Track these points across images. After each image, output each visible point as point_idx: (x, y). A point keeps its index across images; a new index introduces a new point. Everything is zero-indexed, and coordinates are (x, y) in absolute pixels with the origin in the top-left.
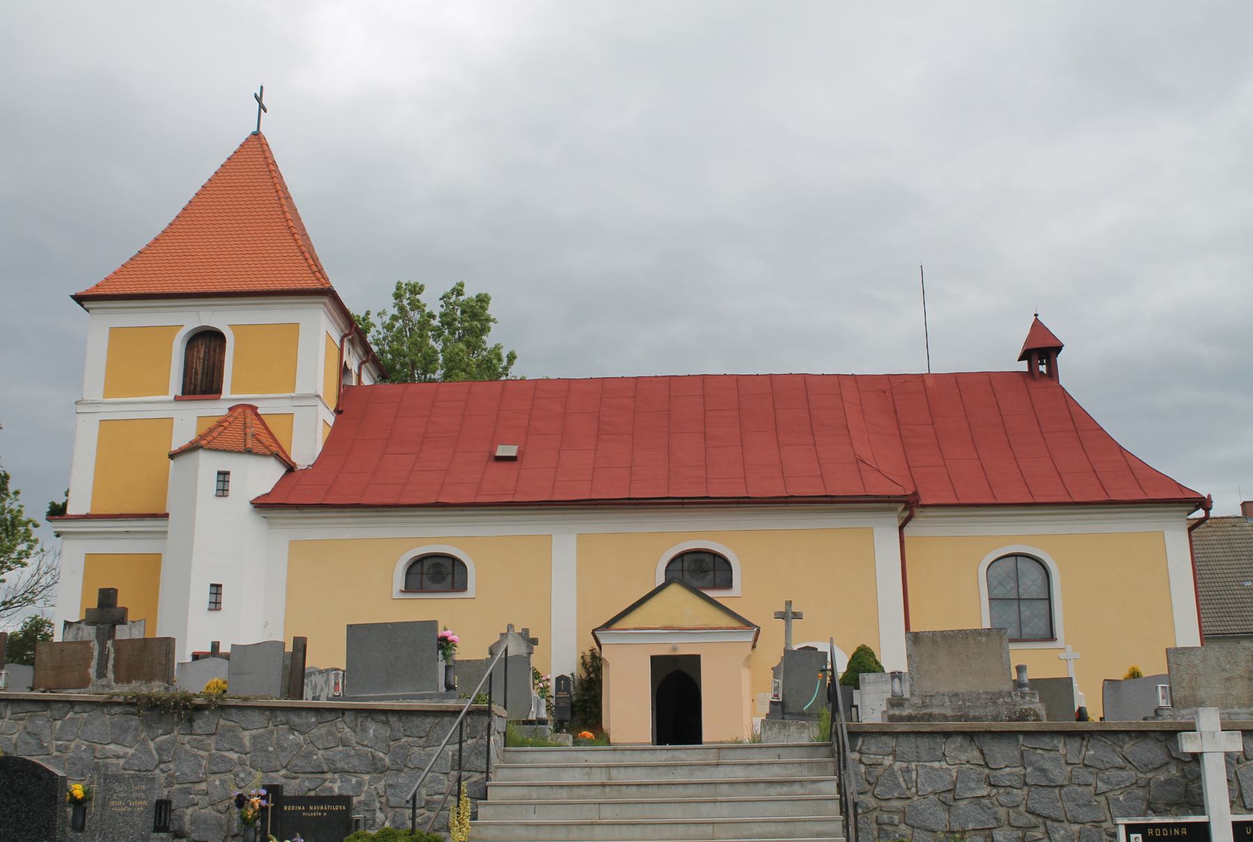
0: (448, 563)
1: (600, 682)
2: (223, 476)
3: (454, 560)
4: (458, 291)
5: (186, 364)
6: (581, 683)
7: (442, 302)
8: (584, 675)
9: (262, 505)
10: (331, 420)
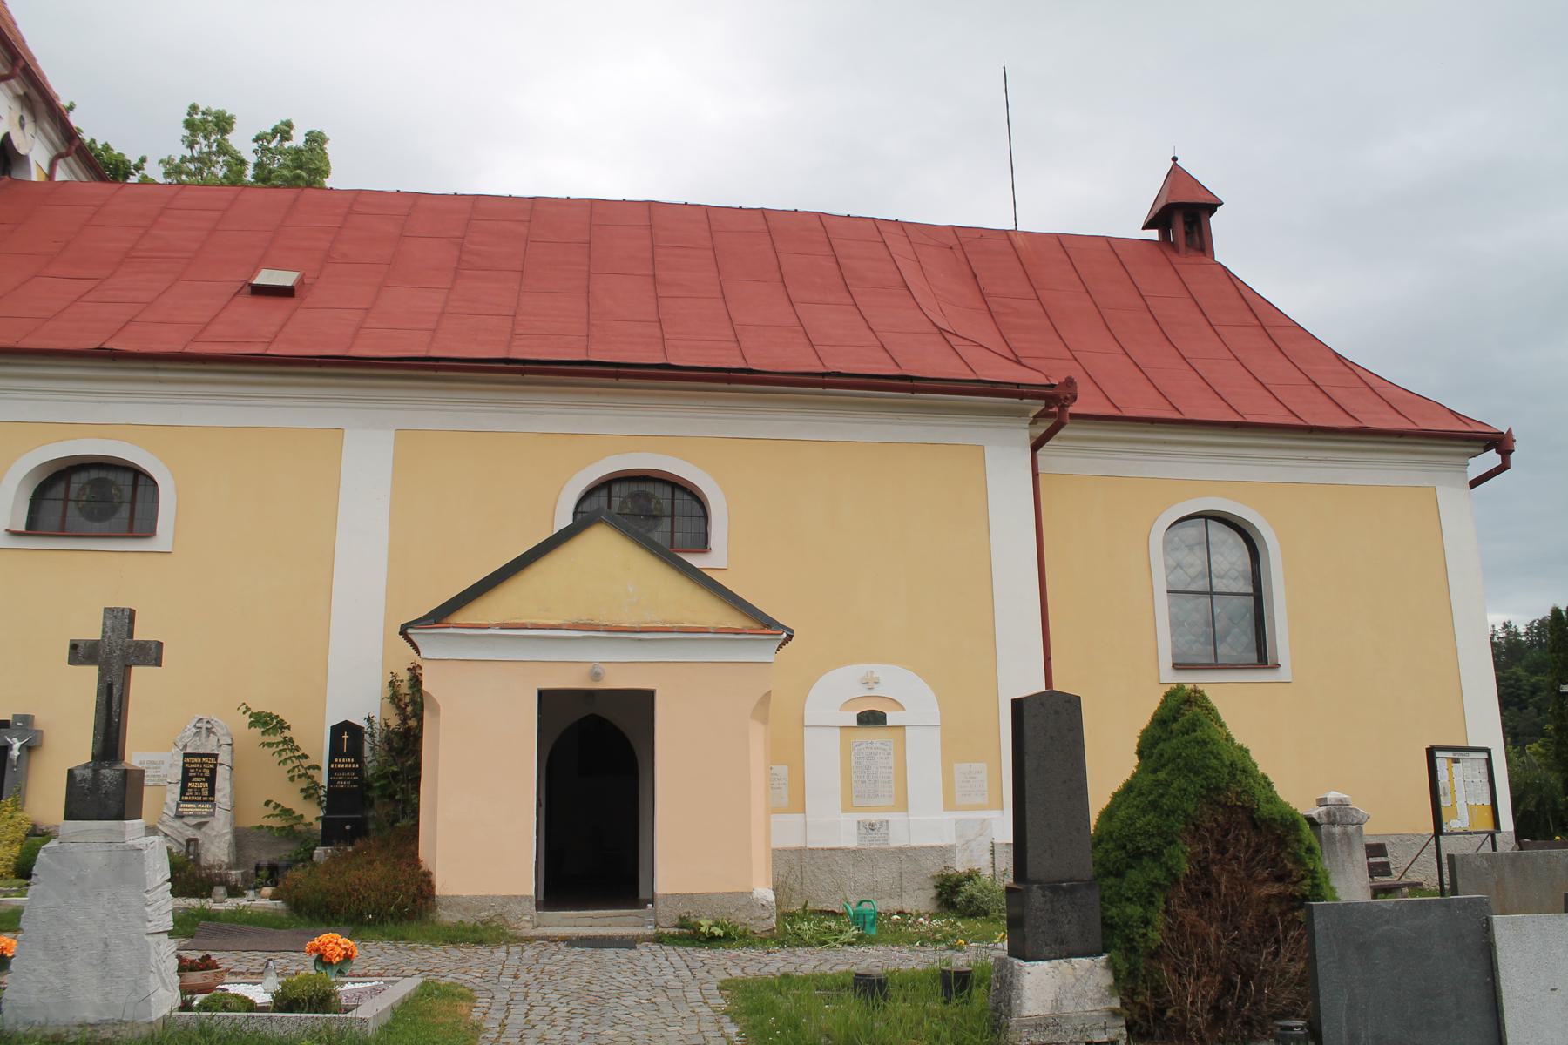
1: (418, 738)
3: (138, 475)
4: (284, 131)
6: (388, 740)
7: (256, 146)
8: (394, 722)
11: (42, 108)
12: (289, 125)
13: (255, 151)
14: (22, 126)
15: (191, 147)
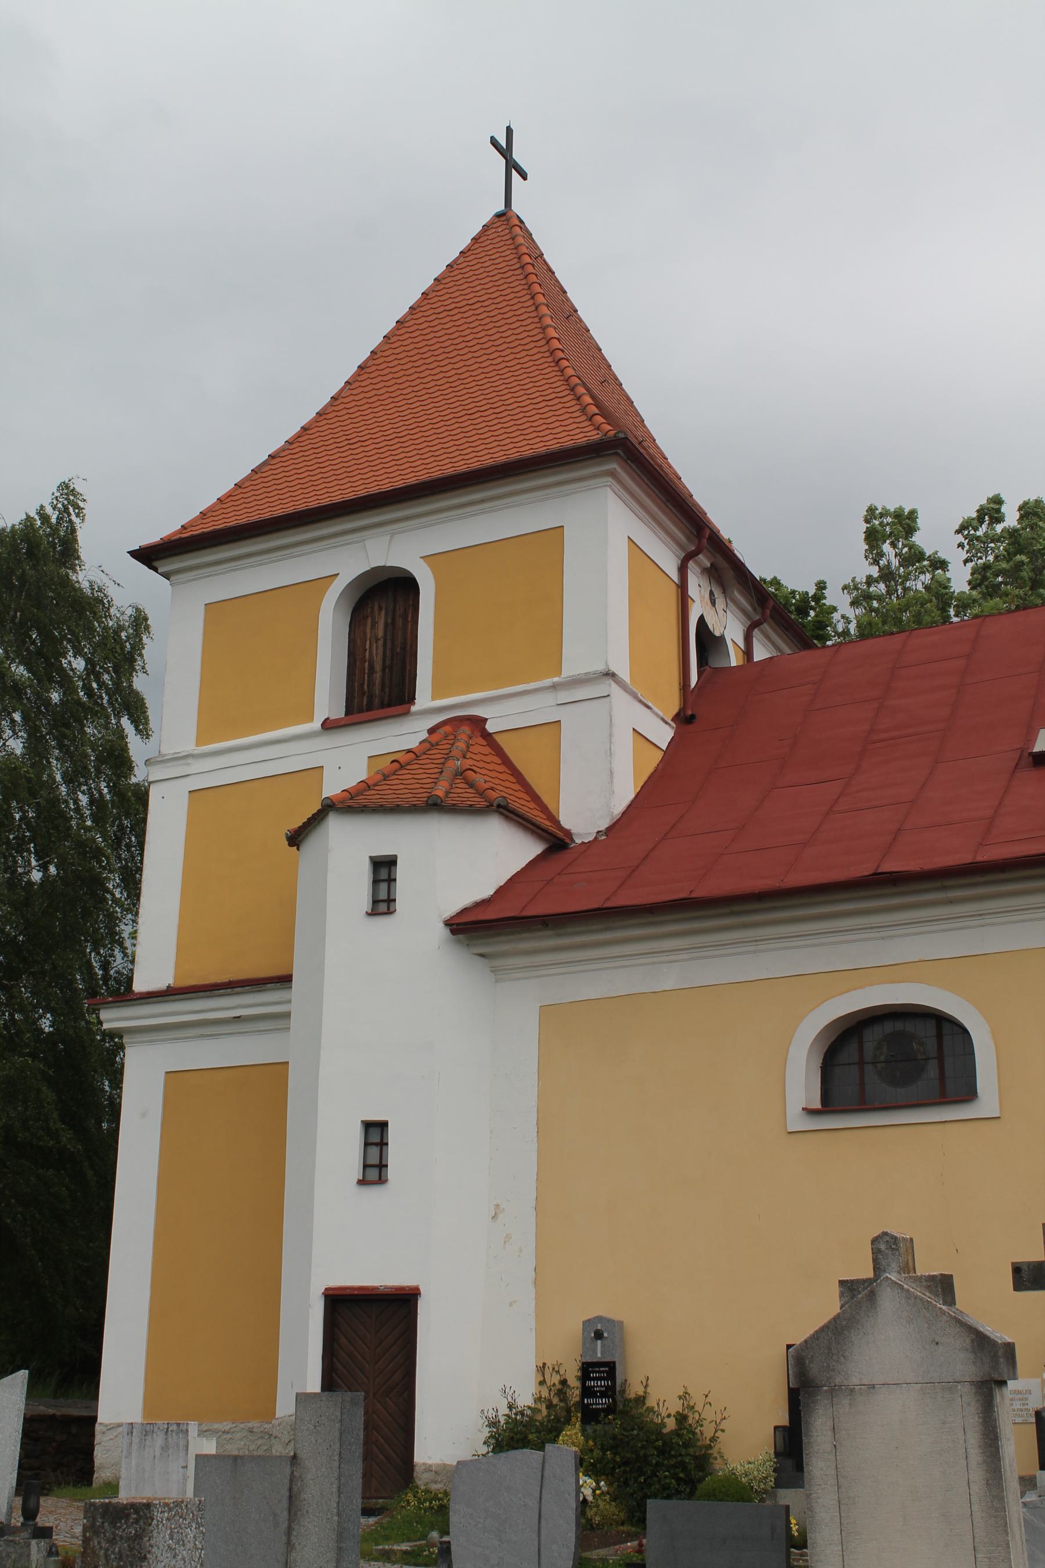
0: (926, 1030)
2: (384, 868)
4: (992, 511)
5: (351, 654)
7: (960, 538)
9: (470, 927)
10: (663, 735)
11: (729, 574)
12: (997, 501)
13: (961, 545)
14: (713, 603)
15: (876, 562)
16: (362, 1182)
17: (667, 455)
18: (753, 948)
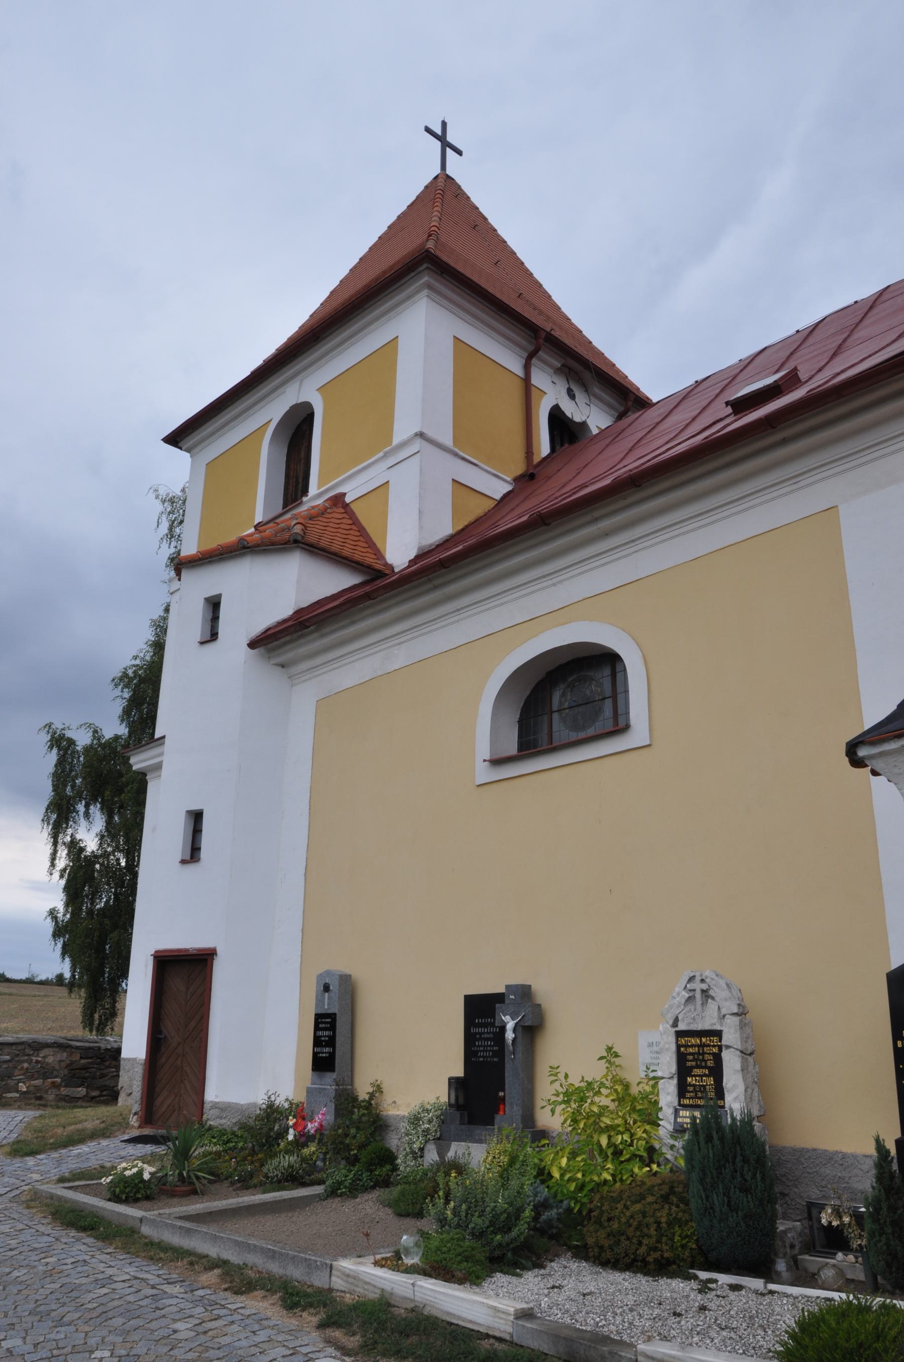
2: (214, 604)
16: (183, 862)
17: (570, 317)
18: (457, 618)
